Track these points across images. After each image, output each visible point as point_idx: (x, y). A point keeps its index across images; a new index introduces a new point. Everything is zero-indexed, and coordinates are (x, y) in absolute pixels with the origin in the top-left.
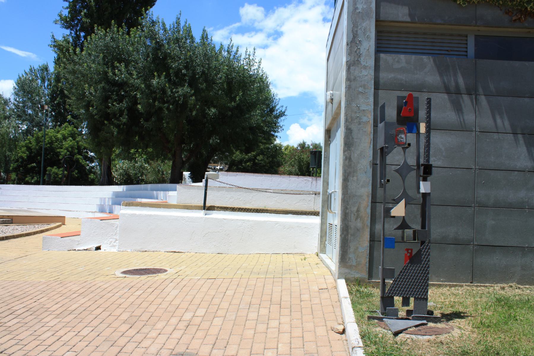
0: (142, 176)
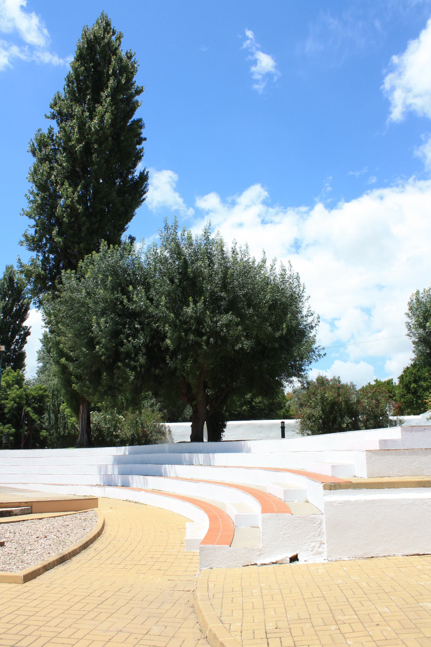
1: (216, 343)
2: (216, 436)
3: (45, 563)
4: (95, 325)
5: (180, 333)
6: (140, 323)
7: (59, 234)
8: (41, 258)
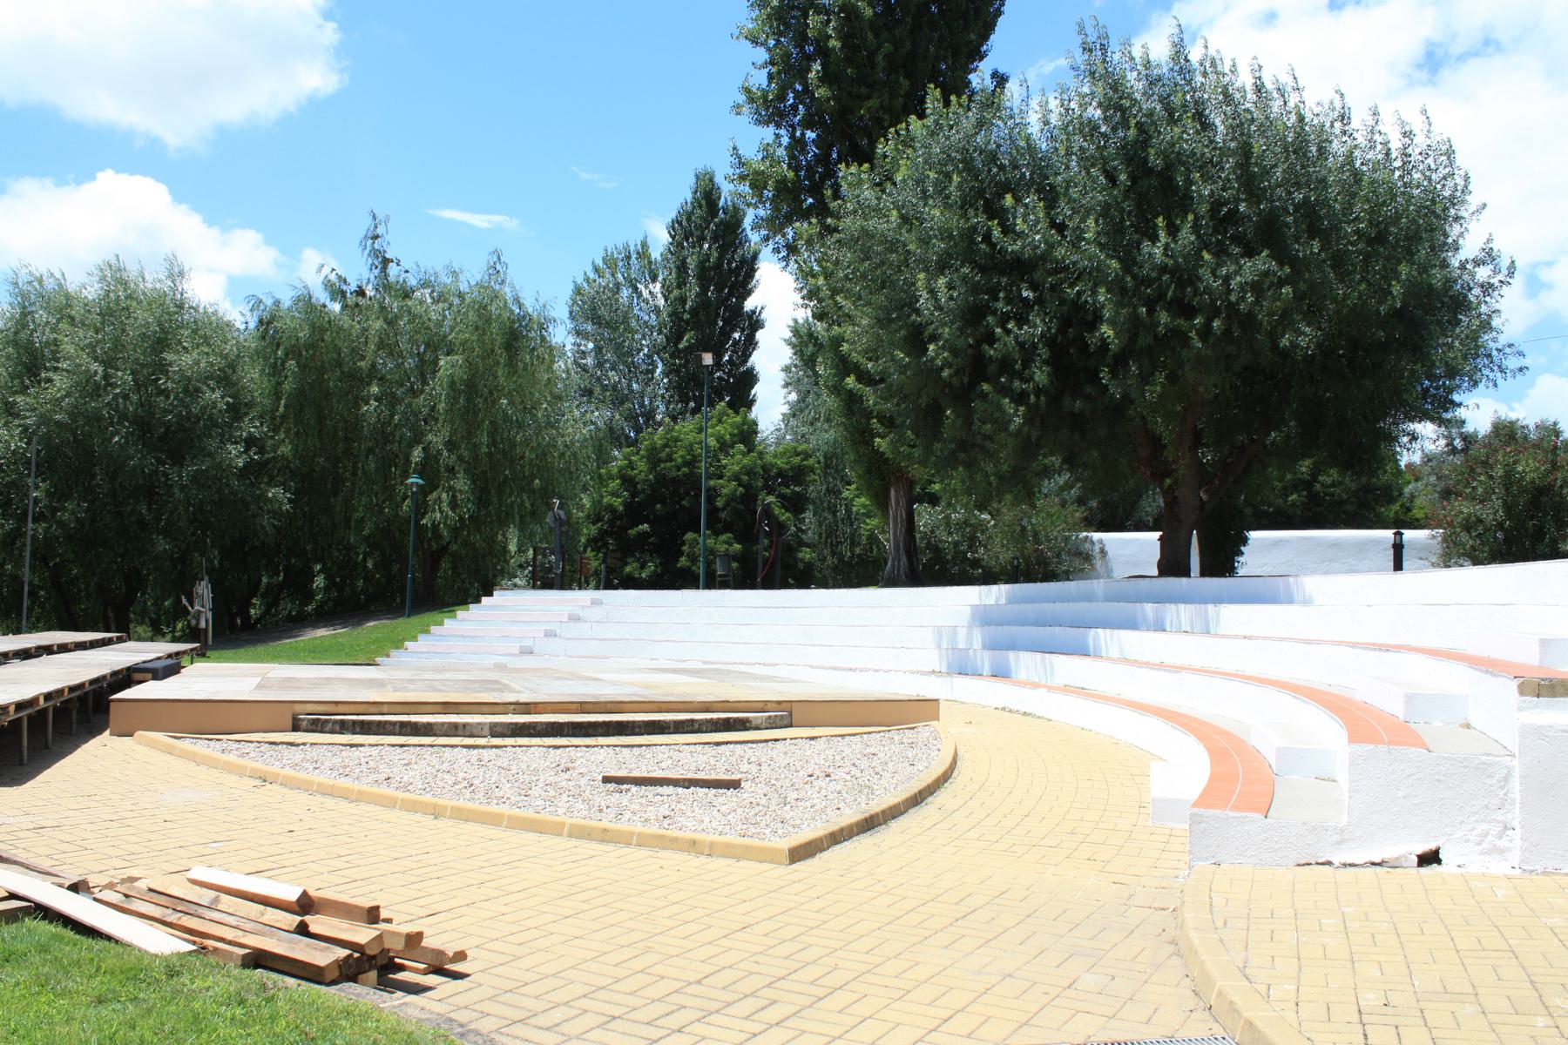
0: (971, 547)
1: (1227, 332)
2: (1221, 562)
3: (834, 827)
4: (925, 295)
5: (1135, 308)
6: (1034, 287)
7: (825, 78)
8: (785, 140)
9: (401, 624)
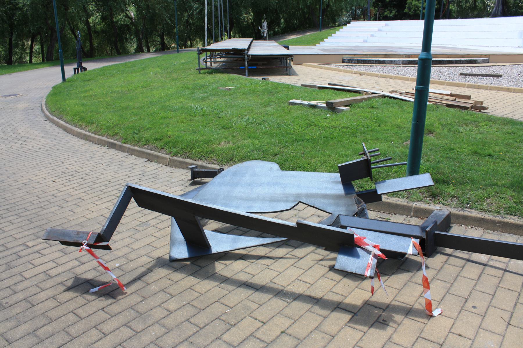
9: (325, 32)
